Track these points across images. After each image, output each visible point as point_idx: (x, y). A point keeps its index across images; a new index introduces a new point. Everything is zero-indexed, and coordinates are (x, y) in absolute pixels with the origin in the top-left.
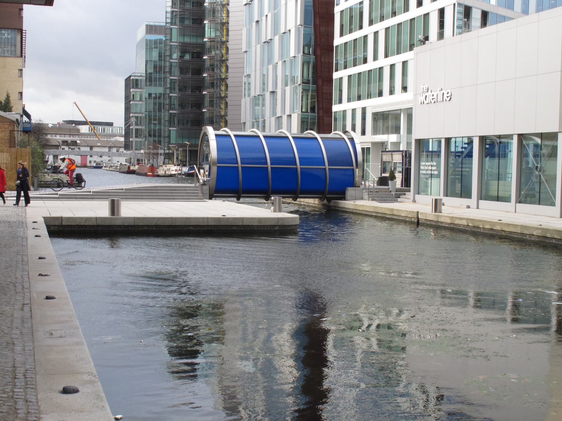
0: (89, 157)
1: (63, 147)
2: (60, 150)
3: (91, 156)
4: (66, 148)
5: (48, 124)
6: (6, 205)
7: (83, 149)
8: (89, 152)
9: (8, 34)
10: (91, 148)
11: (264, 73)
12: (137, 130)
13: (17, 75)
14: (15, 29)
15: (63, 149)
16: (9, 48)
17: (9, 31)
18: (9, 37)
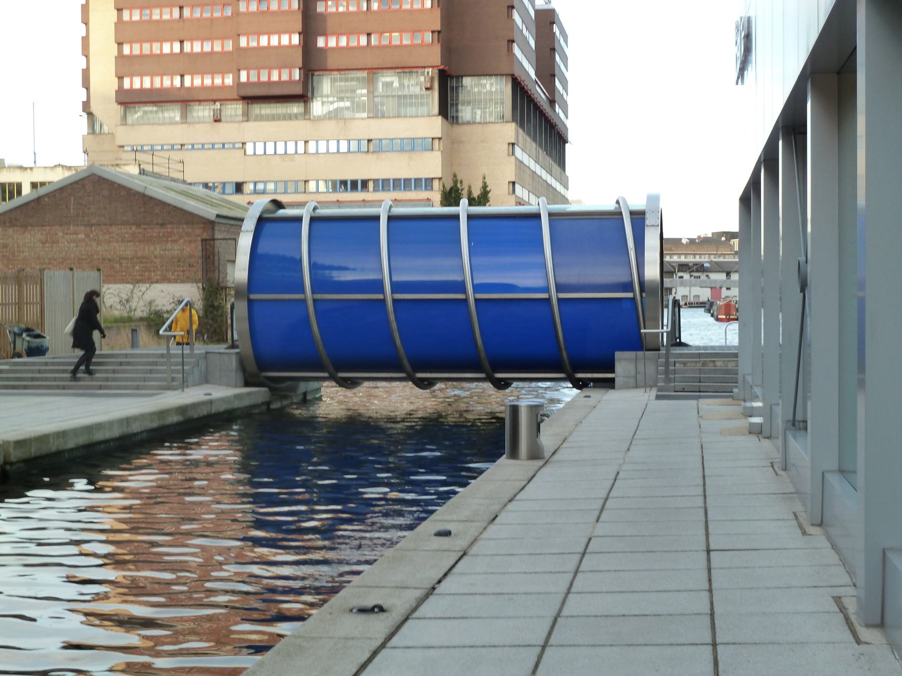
0: (724, 289)
1: (680, 274)
2: (676, 278)
3: (728, 289)
4: (686, 276)
5: (681, 239)
6: (86, 281)
7: (714, 276)
8: (725, 281)
9: (492, 84)
10: (728, 274)
11: (126, 148)
12: (456, 217)
13: (506, 152)
14: (502, 75)
15: (681, 277)
16: (492, 108)
17: (493, 79)
18: (493, 89)
